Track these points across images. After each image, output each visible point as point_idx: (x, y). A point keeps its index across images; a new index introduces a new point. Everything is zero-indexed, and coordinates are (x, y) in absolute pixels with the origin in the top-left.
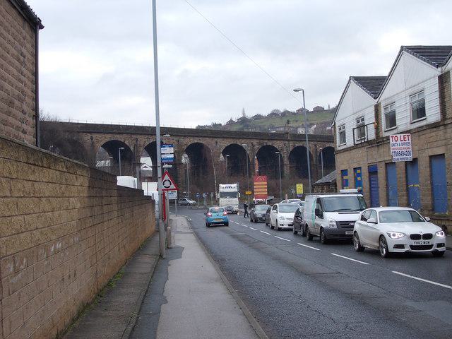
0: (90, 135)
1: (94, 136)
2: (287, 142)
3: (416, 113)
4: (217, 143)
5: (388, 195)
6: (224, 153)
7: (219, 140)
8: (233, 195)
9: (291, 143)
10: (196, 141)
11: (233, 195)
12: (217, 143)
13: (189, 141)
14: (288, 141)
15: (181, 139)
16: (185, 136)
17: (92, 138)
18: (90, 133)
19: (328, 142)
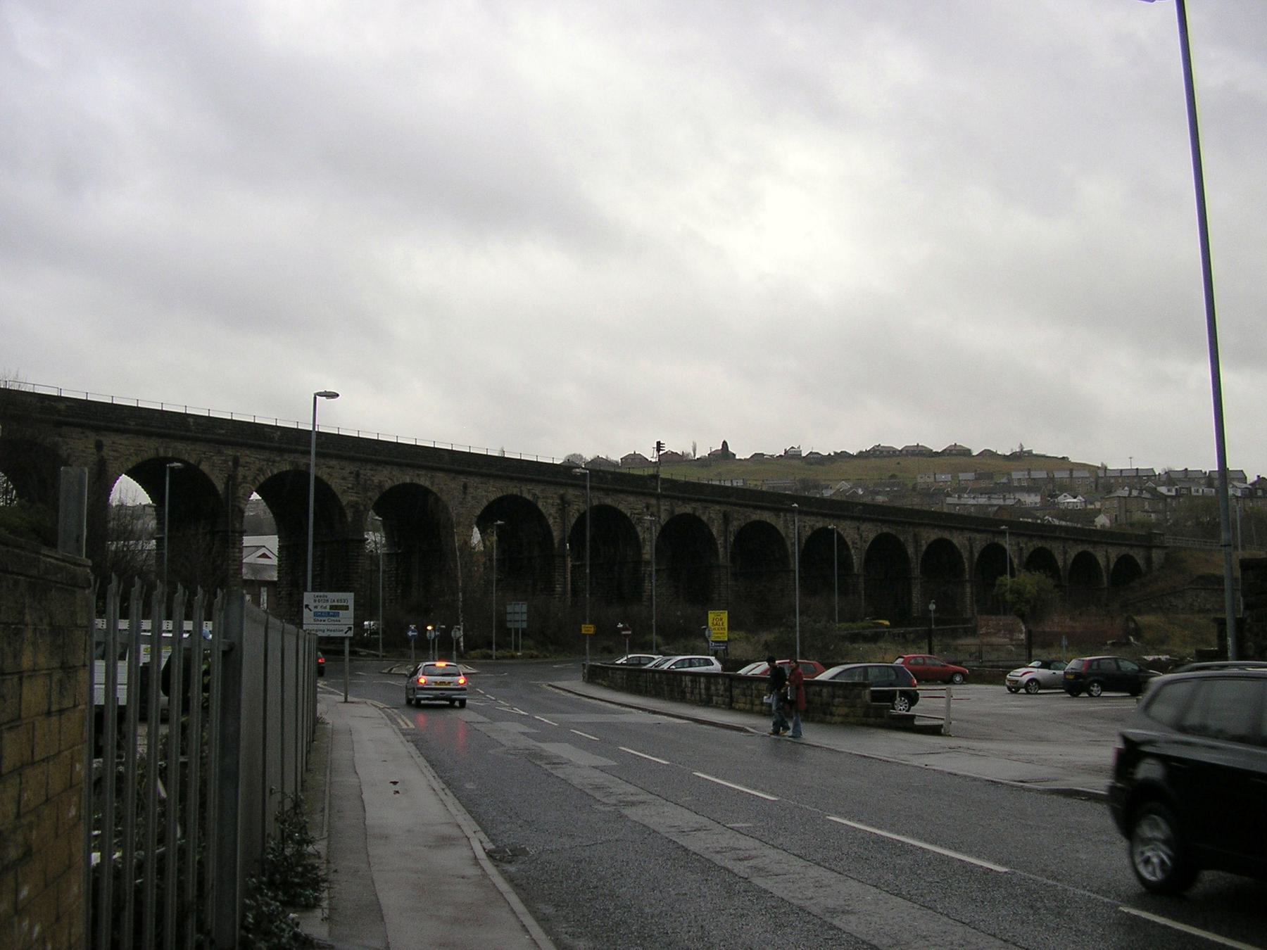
0: (93, 437)
1: (107, 440)
2: (653, 501)
3: (211, 672)
4: (465, 487)
5: (873, 758)
6: (484, 521)
7: (473, 481)
8: (145, 631)
9: (665, 505)
10: (408, 480)
11: (145, 631)
12: (465, 487)
13: (388, 478)
14: (658, 497)
15: (367, 472)
16: (378, 463)
17: (99, 446)
18: (97, 429)
19: (756, 507)
